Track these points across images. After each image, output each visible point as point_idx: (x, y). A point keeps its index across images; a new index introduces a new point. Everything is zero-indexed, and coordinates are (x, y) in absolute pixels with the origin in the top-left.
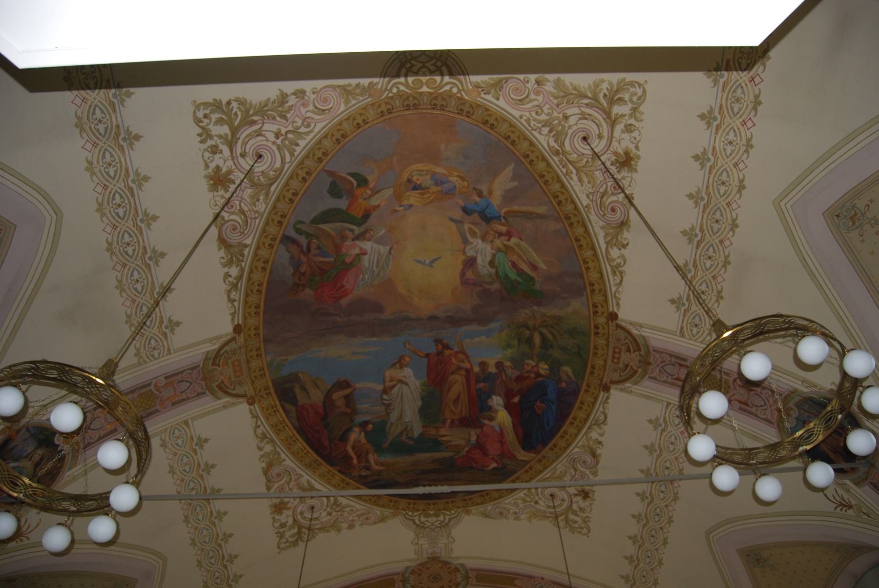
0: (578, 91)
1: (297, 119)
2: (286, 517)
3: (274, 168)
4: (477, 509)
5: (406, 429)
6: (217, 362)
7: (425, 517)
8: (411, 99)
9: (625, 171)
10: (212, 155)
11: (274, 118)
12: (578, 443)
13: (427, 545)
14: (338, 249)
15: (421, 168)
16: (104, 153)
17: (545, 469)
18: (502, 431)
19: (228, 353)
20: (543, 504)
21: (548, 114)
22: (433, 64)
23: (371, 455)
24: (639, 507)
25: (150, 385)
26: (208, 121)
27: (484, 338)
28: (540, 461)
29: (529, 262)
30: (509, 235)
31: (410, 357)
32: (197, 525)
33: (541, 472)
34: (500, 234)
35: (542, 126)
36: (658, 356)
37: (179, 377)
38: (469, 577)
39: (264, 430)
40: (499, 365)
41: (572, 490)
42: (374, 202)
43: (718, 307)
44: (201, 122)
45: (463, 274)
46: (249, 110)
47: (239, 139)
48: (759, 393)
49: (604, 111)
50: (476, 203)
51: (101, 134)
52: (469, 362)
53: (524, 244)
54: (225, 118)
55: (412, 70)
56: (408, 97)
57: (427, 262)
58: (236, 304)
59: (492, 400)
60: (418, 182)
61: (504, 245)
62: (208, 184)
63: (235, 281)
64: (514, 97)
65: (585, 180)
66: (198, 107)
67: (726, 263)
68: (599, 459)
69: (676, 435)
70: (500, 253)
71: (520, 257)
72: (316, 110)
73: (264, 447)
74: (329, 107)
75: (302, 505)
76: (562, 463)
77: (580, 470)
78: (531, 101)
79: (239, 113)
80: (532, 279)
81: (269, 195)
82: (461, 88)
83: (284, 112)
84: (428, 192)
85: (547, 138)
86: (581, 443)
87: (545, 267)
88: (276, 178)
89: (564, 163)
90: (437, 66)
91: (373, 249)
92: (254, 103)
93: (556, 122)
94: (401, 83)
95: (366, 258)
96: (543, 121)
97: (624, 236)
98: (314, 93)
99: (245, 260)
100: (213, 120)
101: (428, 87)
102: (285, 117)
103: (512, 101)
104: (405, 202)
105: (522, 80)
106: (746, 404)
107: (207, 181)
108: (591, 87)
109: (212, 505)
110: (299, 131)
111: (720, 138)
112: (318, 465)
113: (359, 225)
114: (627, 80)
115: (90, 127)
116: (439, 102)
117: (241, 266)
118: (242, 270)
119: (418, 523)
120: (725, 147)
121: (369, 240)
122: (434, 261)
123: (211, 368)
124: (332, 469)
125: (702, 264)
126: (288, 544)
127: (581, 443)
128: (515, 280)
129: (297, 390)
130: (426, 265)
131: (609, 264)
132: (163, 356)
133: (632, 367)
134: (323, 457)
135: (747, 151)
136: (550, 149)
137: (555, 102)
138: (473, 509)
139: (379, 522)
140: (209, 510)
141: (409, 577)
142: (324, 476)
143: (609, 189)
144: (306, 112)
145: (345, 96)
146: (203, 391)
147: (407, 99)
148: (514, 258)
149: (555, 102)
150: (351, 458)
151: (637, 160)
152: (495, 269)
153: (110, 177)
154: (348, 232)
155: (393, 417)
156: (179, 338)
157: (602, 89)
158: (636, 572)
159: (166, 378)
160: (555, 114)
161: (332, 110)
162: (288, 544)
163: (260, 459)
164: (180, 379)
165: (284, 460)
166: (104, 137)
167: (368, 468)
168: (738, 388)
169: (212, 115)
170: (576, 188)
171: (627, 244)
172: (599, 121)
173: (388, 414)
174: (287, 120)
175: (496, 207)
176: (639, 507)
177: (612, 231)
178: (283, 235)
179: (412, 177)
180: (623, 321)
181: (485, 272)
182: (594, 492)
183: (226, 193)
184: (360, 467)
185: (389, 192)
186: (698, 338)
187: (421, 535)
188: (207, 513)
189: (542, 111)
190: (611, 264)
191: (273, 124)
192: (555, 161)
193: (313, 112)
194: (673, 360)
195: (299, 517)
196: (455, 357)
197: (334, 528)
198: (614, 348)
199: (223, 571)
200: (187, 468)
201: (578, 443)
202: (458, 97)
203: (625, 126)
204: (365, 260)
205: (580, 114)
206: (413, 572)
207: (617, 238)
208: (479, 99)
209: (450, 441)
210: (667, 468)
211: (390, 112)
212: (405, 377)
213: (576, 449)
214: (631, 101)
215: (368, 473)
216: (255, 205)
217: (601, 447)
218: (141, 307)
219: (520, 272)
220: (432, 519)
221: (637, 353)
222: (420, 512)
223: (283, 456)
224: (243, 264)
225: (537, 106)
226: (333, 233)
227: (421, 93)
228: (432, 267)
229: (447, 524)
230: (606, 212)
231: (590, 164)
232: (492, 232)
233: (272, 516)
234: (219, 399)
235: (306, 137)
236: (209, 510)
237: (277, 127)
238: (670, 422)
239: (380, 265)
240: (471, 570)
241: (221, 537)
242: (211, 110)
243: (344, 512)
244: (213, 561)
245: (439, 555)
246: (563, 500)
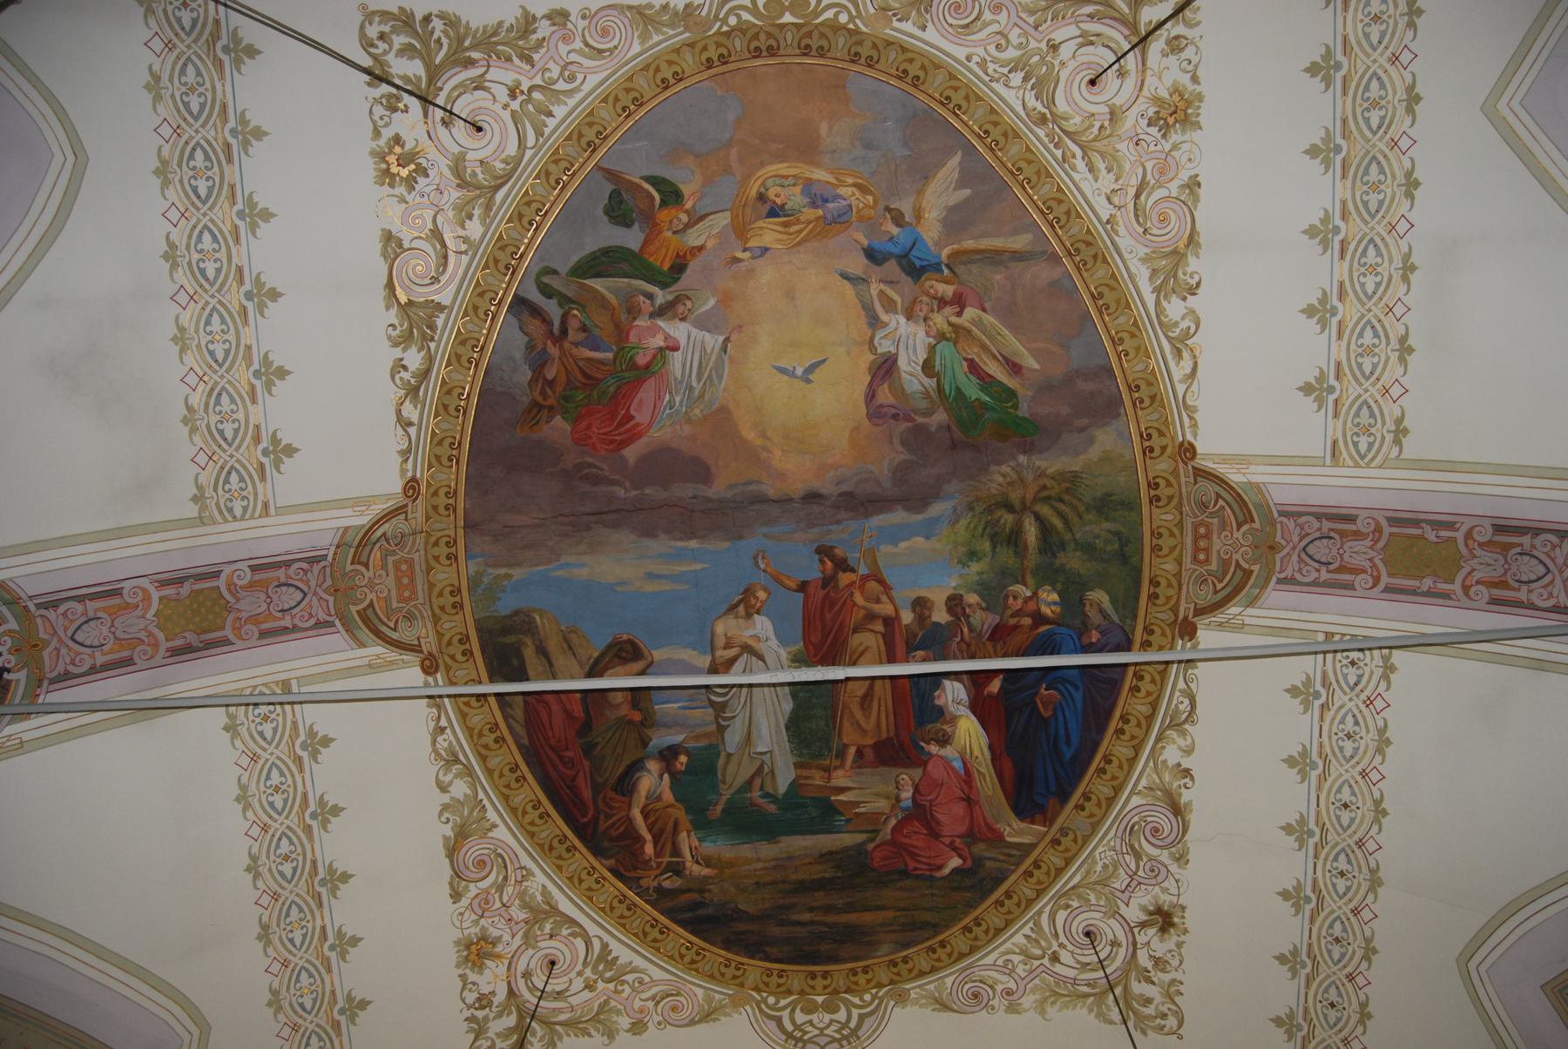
1: (551, 65)
2: (492, 978)
3: (503, 156)
5: (761, 769)
7: (806, 1011)
8: (763, 37)
9: (1176, 132)
10: (388, 113)
11: (509, 59)
12: (1136, 784)
14: (621, 334)
15: (783, 172)
16: (185, 65)
19: (387, 540)
20: (1072, 962)
21: (1020, 46)
24: (1298, 728)
25: (216, 575)
30: (959, 302)
31: (765, 589)
33: (1060, 871)
34: (942, 302)
35: (1010, 72)
36: (1291, 524)
39: (454, 742)
40: (955, 603)
41: (1134, 913)
42: (694, 238)
43: (1388, 688)
44: (372, 45)
45: (871, 396)
46: (464, 39)
47: (441, 89)
48: (1527, 547)
49: (1122, 21)
50: (891, 239)
51: (183, 29)
52: (891, 600)
53: (992, 319)
57: (799, 372)
58: (413, 431)
59: (944, 690)
60: (778, 201)
61: (950, 324)
64: (954, 22)
66: (369, 16)
67: (1408, 269)
69: (1356, 712)
70: (944, 342)
71: (984, 347)
72: (587, 50)
73: (451, 783)
74: (611, 45)
75: (531, 952)
77: (1147, 855)
78: (986, 25)
79: (445, 41)
80: (1012, 394)
82: (854, 13)
84: (798, 221)
87: (1036, 366)
88: (508, 176)
91: (692, 340)
92: (473, 26)
93: (1037, 58)
96: (1011, 61)
97: (1189, 270)
98: (584, 17)
99: (436, 338)
100: (396, 46)
102: (529, 60)
103: (950, 30)
104: (752, 243)
106: (1502, 584)
107: (375, 163)
111: (1355, 16)
113: (664, 286)
115: (165, 11)
116: (815, 42)
117: (429, 348)
118: (430, 359)
120: (1367, 30)
121: (683, 319)
123: (349, 567)
124: (596, 864)
125: (1334, 818)
127: (1143, 783)
131: (1167, 336)
132: (252, 518)
133: (1238, 565)
135: (1376, 820)
136: (1027, 115)
137: (1031, 20)
138: (913, 988)
139: (700, 1021)
140: (319, 923)
142: (581, 881)
143: (1149, 176)
147: (756, 37)
148: (973, 352)
149: (1031, 20)
150: (639, 839)
153: (191, 113)
154: (642, 298)
155: (733, 739)
156: (289, 484)
159: (254, 568)
160: (1033, 44)
163: (441, 814)
164: (283, 580)
165: (494, 826)
166: (188, 34)
167: (677, 870)
168: (1478, 552)
169: (394, 37)
170: (1086, 187)
171: (1198, 284)
172: (1117, 43)
173: (721, 730)
174: (533, 66)
175: (930, 243)
176: (1298, 728)
180: (1208, 456)
181: (916, 387)
184: (659, 864)
185: (722, 220)
186: (1374, 458)
188: (314, 928)
189: (1008, 41)
190: (1170, 334)
192: (1037, 138)
193: (580, 52)
194: (1327, 525)
195: (521, 983)
196: (862, 588)
198: (1196, 527)
200: (278, 800)
201: (1136, 784)
202: (849, 30)
203: (1168, 42)
204: (676, 359)
207: (1175, 276)
208: (888, 31)
209: (857, 804)
210: (1346, 806)
211: (724, 60)
212: (757, 638)
213: (1133, 802)
216: (463, 227)
217: (1190, 784)
218: (220, 394)
219: (986, 380)
223: (491, 815)
224: (433, 345)
227: (784, 26)
228: (808, 381)
229: (855, 1032)
231: (1108, 132)
232: (925, 299)
233: (460, 971)
234: (363, 645)
236: (319, 923)
237: (515, 76)
238: (1337, 681)
239: (706, 376)
243: (623, 982)
246: (1115, 944)
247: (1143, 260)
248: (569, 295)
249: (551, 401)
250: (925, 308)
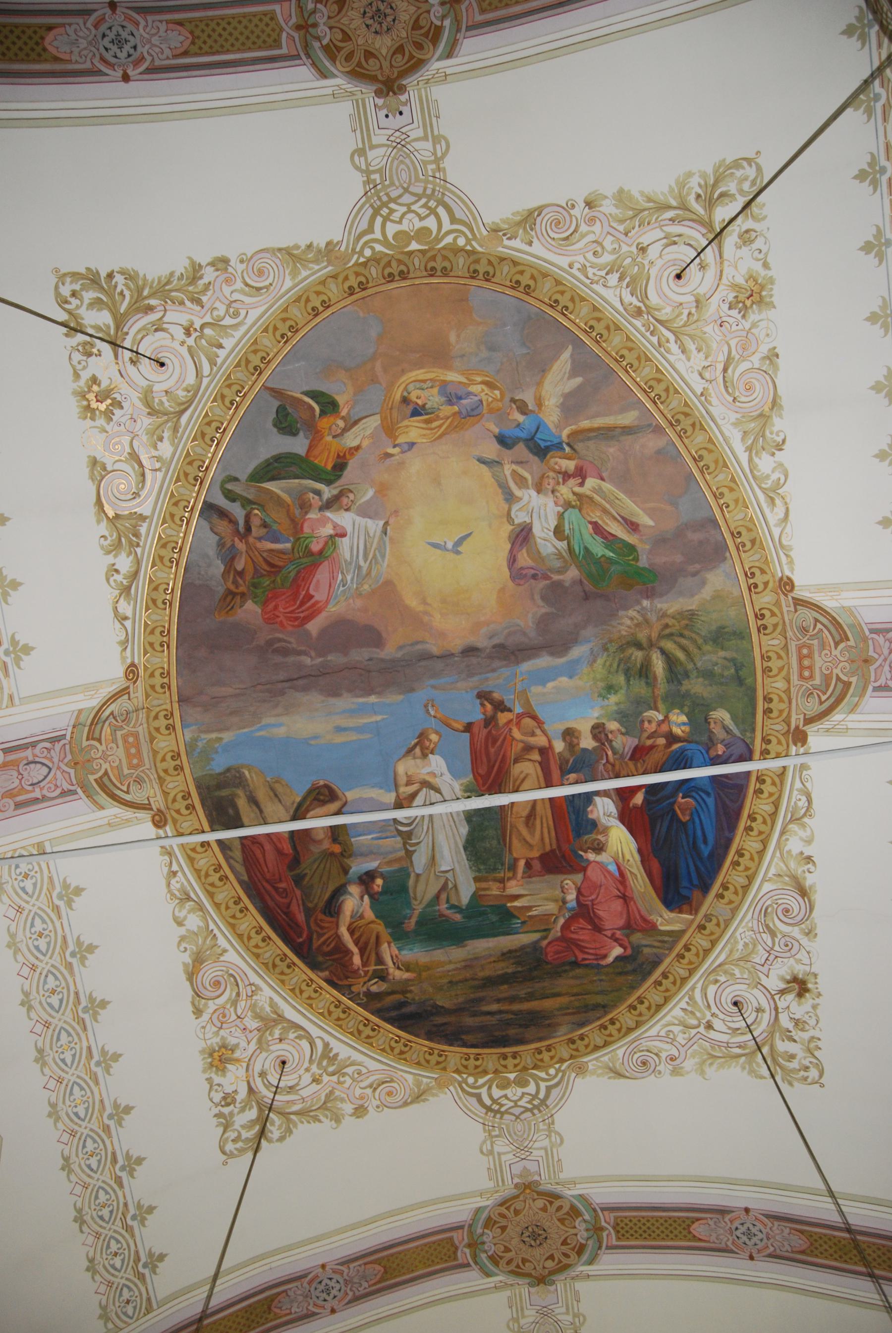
0: (654, 202)
1: (218, 304)
3: (184, 385)
4: (596, 1059)
5: (444, 887)
9: (753, 312)
13: (511, 1156)
14: (297, 527)
15: (421, 377)
17: (714, 943)
18: (622, 874)
19: (115, 718)
22: (425, 206)
23: (386, 945)
26: (78, 302)
27: (564, 679)
28: (701, 927)
29: (623, 518)
30: (581, 474)
31: (437, 733)
33: (707, 952)
35: (607, 274)
37: (29, 753)
38: (602, 1229)
39: (186, 883)
40: (598, 731)
42: (351, 440)
44: (67, 302)
45: (512, 560)
46: (143, 289)
47: (127, 334)
50: (518, 425)
52: (544, 732)
54: (105, 299)
56: (390, 262)
57: (450, 545)
58: (128, 624)
59: (595, 805)
60: (420, 402)
61: (574, 493)
63: (125, 582)
64: (556, 236)
66: (62, 278)
70: (570, 510)
71: (605, 511)
72: (247, 289)
73: (185, 918)
74: (267, 283)
75: (264, 1054)
76: (744, 924)
78: (583, 236)
79: (127, 293)
80: (632, 548)
82: (470, 236)
84: (438, 418)
85: (618, 293)
86: (773, 871)
87: (651, 523)
90: (429, 208)
92: (149, 278)
94: (376, 241)
95: (345, 541)
97: (775, 429)
98: (242, 261)
99: (141, 544)
100: (86, 301)
101: (419, 242)
103: (553, 243)
104: (401, 440)
113: (329, 483)
114: (728, 162)
118: (138, 562)
119: (488, 1102)
124: (313, 976)
126: (240, 1145)
127: (773, 871)
128: (603, 556)
129: (242, 803)
131: (760, 488)
133: (838, 678)
134: (298, 950)
136: (625, 309)
137: (621, 228)
138: (591, 1061)
139: (412, 1103)
141: (482, 1234)
142: (301, 992)
143: (734, 353)
145: (291, 263)
147: (389, 264)
148: (596, 516)
149: (621, 228)
150: (348, 952)
154: (311, 495)
155: (420, 861)
157: (691, 188)
160: (625, 248)
162: (240, 1145)
164: (31, 758)
165: (225, 951)
167: (382, 976)
169: (84, 293)
170: (680, 366)
171: (784, 441)
173: (409, 854)
174: (203, 307)
175: (551, 426)
177: (753, 425)
178: (205, 502)
184: (366, 973)
185: (373, 423)
188: (81, 1049)
189: (603, 248)
190: (763, 486)
192: (636, 328)
193: (242, 292)
195: (259, 1081)
196: (518, 724)
198: (799, 649)
202: (467, 252)
203: (740, 236)
204: (344, 544)
206: (489, 1223)
207: (763, 436)
208: (500, 249)
209: (529, 908)
211: (363, 286)
212: (433, 774)
214: (741, 192)
215: (383, 987)
216: (155, 448)
220: (514, 1092)
221: (842, 645)
222: (489, 1076)
223: (222, 942)
227: (411, 253)
231: (695, 318)
232: (551, 474)
233: (207, 1076)
240: (603, 1209)
241: (132, 1211)
243: (344, 1075)
245: (536, 1178)
246: (759, 1010)
247: (735, 425)
248: (250, 497)
249: (242, 589)
250: (552, 482)
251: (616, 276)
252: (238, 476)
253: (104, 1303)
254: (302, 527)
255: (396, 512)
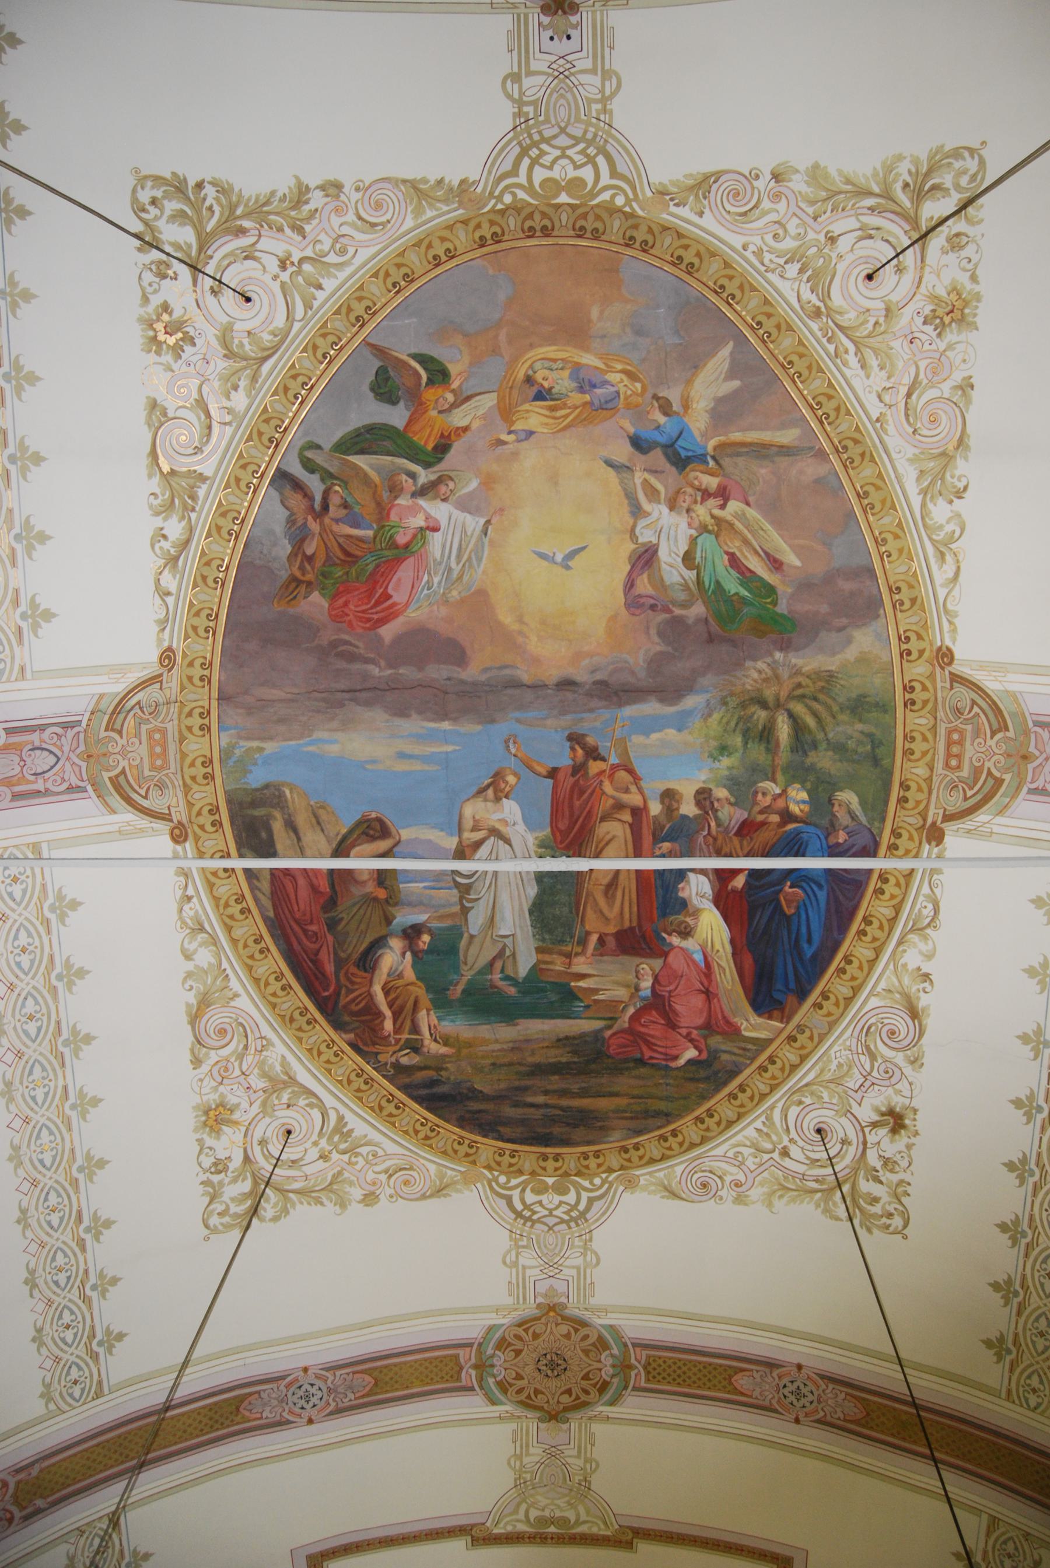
0: (854, 185)
1: (322, 237)
5: (501, 954)
6: (117, 726)
8: (537, 217)
10: (157, 280)
13: (537, 1271)
14: (383, 512)
15: (552, 355)
20: (802, 1158)
22: (583, 152)
23: (424, 1012)
26: (157, 212)
27: (671, 733)
28: (792, 1039)
30: (723, 494)
31: (515, 774)
32: (39, 1177)
34: (706, 494)
35: (786, 263)
37: (35, 737)
39: (201, 912)
40: (703, 797)
41: (866, 1113)
42: (459, 418)
44: (144, 210)
45: (630, 584)
46: (237, 206)
47: (211, 257)
50: (658, 427)
52: (640, 790)
55: (541, 161)
56: (533, 213)
57: (559, 558)
58: (170, 600)
59: (688, 882)
60: (546, 384)
61: (713, 516)
62: (142, 336)
65: (873, 362)
66: (142, 181)
68: (924, 1022)
70: (705, 535)
71: (746, 542)
72: (359, 223)
73: (195, 951)
74: (384, 219)
76: (841, 1041)
79: (217, 209)
80: (770, 590)
81: (257, 382)
82: (631, 196)
83: (298, 220)
84: (564, 406)
85: (796, 287)
86: (883, 985)
88: (275, 349)
89: (830, 334)
90: (587, 156)
92: (246, 194)
97: (957, 473)
98: (357, 189)
99: (197, 509)
100: (168, 212)
102: (300, 231)
103: (727, 217)
104: (518, 426)
105: (748, 175)
108: (878, 174)
109: (89, 1255)
110: (323, 259)
112: (309, 1023)
113: (427, 465)
114: (947, 149)
116: (590, 224)
118: (191, 530)
119: (519, 1207)
122: (571, 555)
123: (103, 734)
126: (227, 1219)
127: (883, 985)
128: (737, 594)
129: (278, 826)
130: (556, 563)
131: (930, 539)
136: (802, 308)
137: (810, 210)
139: (431, 1196)
141: (492, 1356)
142: (320, 1053)
143: (922, 376)
144: (341, 225)
145: (415, 199)
146: (80, 784)
147: (531, 216)
148: (734, 546)
149: (810, 210)
150: (379, 1014)
151: (975, 304)
152: (695, 572)
154: (404, 477)
155: (476, 921)
157: (898, 175)
158: (1014, 1378)
160: (811, 235)
161: (389, 226)
164: (37, 744)
165: (236, 995)
167: (415, 1048)
169: (165, 202)
170: (856, 383)
171: (966, 488)
172: (897, 238)
173: (465, 911)
174: (304, 237)
177: (932, 464)
178: (278, 469)
179: (535, 372)
182: (915, 1111)
183: (176, 362)
184: (398, 1041)
185: (488, 402)
187: (524, 1242)
189: (786, 231)
190: (934, 537)
191: (278, 240)
192: (811, 331)
193: (353, 225)
195: (257, 1149)
196: (611, 777)
197: (333, 1197)
198: (949, 733)
199: (75, 1255)
203: (949, 240)
204: (436, 540)
205: (860, 229)
206: (502, 1344)
207: (943, 479)
208: (665, 216)
209: (596, 991)
211: (497, 238)
212: (504, 822)
214: (957, 187)
215: (414, 1060)
216: (228, 398)
217: (929, 989)
220: (551, 1199)
222: (525, 1177)
223: (234, 984)
224: (193, 515)
225: (775, 222)
226: (373, 474)
227: (559, 206)
228: (568, 568)
229: (583, 1214)
230: (919, 425)
231: (882, 329)
232: (689, 490)
233: (198, 1136)
234: (113, 812)
235: (338, 274)
236: (61, 1083)
240: (634, 1345)
242: (164, 192)
243: (357, 1155)
244: (55, 1219)
245: (563, 1300)
246: (845, 1142)
248: (332, 470)
249: (309, 577)
251: (797, 266)
252: (321, 442)
253: (48, 1380)
254: (388, 514)
255: (502, 510)
